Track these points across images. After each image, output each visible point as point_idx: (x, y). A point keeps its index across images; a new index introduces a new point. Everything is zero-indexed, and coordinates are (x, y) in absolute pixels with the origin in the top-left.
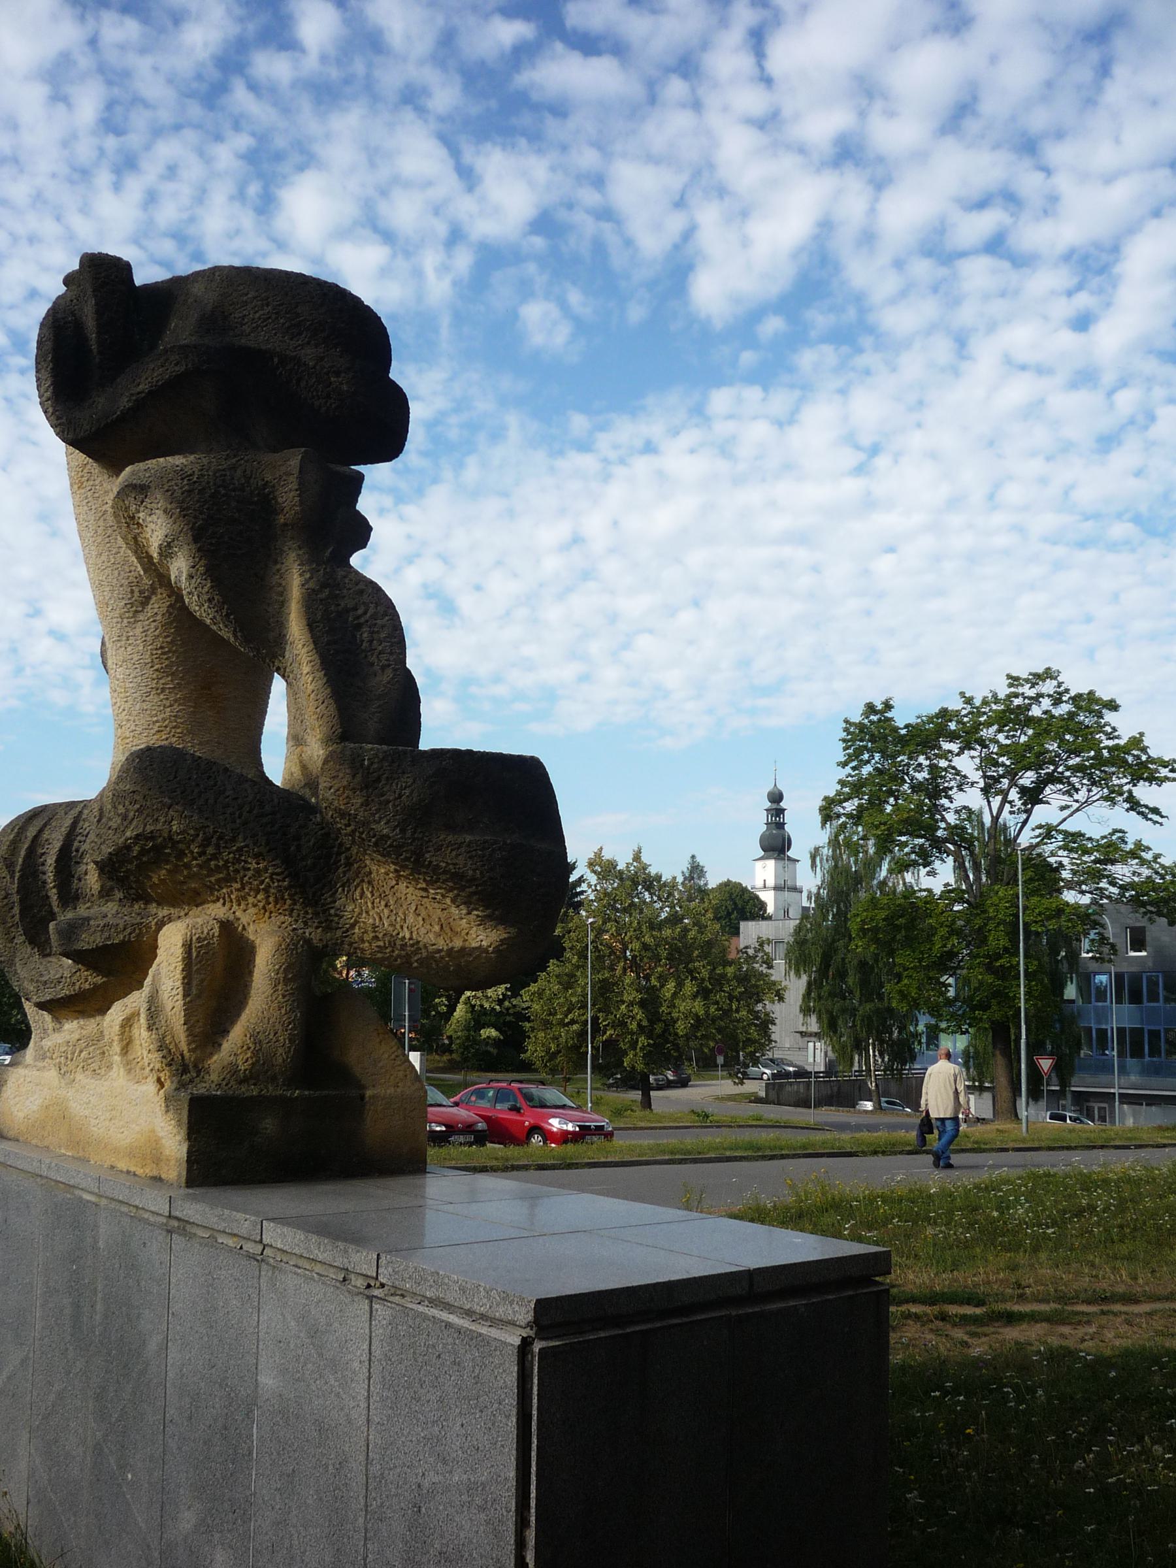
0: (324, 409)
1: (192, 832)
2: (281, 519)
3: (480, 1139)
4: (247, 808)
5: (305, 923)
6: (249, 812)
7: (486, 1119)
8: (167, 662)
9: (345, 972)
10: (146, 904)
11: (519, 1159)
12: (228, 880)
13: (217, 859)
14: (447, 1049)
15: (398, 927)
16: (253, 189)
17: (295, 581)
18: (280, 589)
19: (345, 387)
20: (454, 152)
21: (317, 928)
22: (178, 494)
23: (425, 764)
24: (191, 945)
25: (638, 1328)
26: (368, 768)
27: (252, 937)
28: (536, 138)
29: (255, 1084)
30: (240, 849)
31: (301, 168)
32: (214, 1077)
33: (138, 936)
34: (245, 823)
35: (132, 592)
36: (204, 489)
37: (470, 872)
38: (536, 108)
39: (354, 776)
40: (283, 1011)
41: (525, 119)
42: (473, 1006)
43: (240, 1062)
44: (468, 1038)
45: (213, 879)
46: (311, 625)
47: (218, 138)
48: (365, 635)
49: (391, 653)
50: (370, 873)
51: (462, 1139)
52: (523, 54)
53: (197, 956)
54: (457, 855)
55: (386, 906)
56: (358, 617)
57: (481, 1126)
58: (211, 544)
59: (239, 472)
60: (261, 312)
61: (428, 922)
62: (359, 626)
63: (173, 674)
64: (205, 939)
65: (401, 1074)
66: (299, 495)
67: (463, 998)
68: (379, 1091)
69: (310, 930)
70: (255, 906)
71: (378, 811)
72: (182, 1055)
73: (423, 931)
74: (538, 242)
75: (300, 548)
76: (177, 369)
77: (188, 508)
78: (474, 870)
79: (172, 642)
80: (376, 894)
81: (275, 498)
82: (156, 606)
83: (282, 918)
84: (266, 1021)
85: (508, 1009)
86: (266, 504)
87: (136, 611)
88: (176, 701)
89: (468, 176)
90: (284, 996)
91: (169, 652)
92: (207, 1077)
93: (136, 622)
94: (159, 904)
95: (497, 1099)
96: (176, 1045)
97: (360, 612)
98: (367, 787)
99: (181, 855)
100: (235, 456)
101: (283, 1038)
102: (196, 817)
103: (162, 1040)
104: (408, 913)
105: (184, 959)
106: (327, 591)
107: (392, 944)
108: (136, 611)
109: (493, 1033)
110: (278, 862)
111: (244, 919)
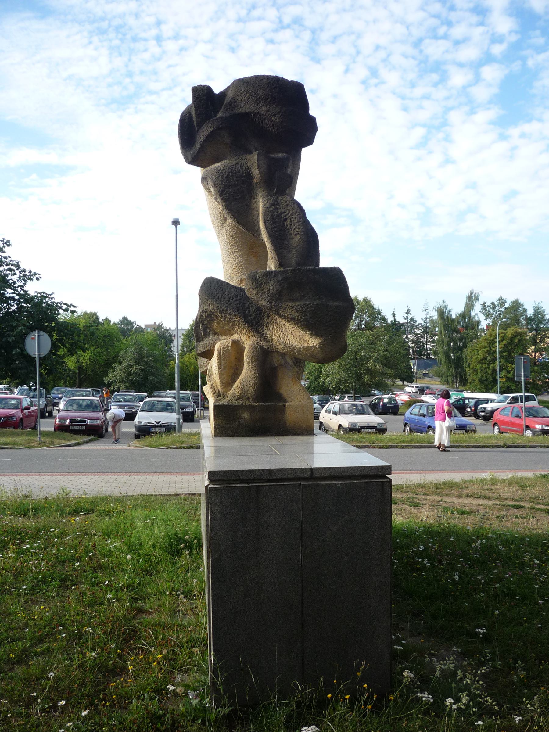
2: (255, 181)
9: (534, 354)
19: (278, 121)
25: (255, 485)
30: (230, 314)
34: (231, 304)
35: (221, 216)
46: (265, 223)
49: (299, 229)
54: (292, 311)
56: (286, 216)
62: (286, 220)
63: (237, 246)
65: (302, 397)
68: (293, 403)
71: (261, 296)
73: (294, 341)
78: (298, 316)
81: (252, 173)
86: (249, 176)
88: (239, 256)
97: (286, 213)
98: (257, 287)
99: (217, 317)
105: (218, 355)
106: (273, 207)
110: (242, 317)
111: (244, 339)
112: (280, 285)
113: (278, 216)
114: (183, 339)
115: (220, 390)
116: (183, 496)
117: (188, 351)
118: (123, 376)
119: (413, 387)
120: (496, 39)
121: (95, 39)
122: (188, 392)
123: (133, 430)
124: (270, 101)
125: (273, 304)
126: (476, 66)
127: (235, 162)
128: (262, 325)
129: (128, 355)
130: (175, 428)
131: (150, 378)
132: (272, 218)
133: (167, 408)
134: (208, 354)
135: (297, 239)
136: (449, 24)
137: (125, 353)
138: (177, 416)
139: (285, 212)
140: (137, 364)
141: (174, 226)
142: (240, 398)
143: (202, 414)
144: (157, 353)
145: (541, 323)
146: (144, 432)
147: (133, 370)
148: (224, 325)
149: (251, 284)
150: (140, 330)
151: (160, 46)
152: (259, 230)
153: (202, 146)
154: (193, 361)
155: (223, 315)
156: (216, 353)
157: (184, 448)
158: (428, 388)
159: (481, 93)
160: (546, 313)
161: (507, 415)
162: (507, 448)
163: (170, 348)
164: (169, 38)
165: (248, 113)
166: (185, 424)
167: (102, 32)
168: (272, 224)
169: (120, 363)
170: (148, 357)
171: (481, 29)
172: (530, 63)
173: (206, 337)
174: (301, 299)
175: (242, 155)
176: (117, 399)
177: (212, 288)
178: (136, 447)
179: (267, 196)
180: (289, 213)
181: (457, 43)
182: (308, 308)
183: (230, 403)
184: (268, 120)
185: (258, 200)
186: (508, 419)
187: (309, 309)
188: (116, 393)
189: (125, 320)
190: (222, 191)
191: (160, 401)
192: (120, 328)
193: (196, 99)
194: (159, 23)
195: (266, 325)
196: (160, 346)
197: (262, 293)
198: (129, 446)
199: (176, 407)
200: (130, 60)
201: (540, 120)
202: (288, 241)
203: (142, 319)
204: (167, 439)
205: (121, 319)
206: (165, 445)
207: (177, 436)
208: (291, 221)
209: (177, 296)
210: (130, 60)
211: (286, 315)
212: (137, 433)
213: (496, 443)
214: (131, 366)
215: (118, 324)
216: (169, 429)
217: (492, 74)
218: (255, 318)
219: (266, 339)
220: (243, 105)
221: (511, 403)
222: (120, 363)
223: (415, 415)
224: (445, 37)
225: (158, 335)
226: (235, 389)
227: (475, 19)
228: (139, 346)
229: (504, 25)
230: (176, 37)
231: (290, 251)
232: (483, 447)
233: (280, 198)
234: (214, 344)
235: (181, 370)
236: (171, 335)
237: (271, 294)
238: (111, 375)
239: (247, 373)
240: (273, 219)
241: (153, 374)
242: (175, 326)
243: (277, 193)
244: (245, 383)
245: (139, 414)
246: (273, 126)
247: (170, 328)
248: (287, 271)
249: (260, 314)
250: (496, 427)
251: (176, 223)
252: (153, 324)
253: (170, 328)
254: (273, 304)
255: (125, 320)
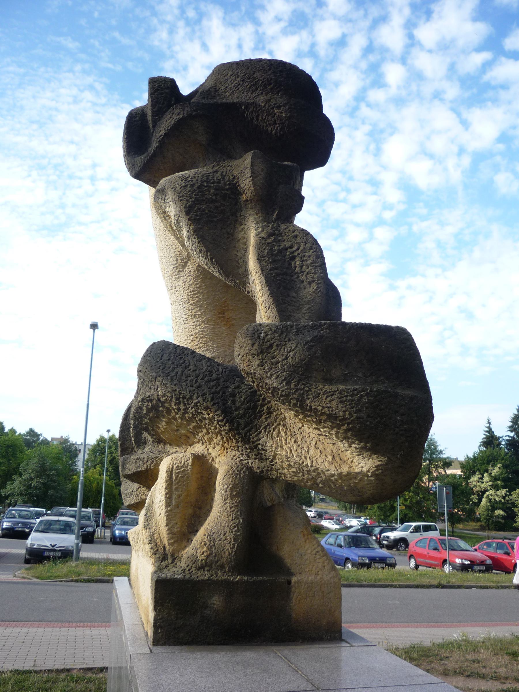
0: (273, 132)
1: (169, 395)
2: (244, 197)
3: (488, 569)
4: (201, 376)
5: (248, 456)
6: (202, 379)
7: (491, 558)
8: (197, 299)
9: (427, 483)
10: (164, 445)
11: (505, 582)
12: (199, 427)
13: (187, 413)
14: (478, 520)
15: (303, 457)
16: (372, 147)
17: (252, 232)
18: (245, 240)
19: (284, 115)
20: (459, 115)
21: (255, 459)
22: (178, 188)
23: (306, 333)
24: (172, 471)
26: (264, 339)
27: (217, 466)
28: (495, 101)
29: (208, 571)
30: (196, 405)
31: (392, 134)
32: (183, 564)
33: (155, 465)
34: (199, 387)
35: (177, 260)
36: (194, 184)
37: (341, 414)
38: (494, 88)
39: (253, 345)
40: (230, 518)
41: (491, 94)
42: (491, 499)
43: (199, 554)
44: (488, 515)
45: (191, 427)
46: (260, 259)
47: (356, 128)
48: (298, 263)
49: (315, 273)
50: (285, 418)
51: (478, 568)
52: (487, 66)
53: (176, 479)
54: (331, 401)
55: (295, 442)
56: (293, 252)
57: (489, 562)
58: (197, 215)
59: (219, 173)
60: (235, 83)
61: (324, 453)
62: (293, 258)
63: (200, 306)
64: (182, 467)
65: (320, 565)
66: (252, 180)
67: (485, 495)
68: (303, 577)
69: (252, 460)
70: (218, 444)
72: (164, 547)
73: (320, 460)
74: (501, 147)
75: (257, 214)
76: (178, 117)
77: (183, 196)
78: (344, 412)
79: (200, 287)
80: (289, 434)
81: (239, 185)
82: (190, 267)
83: (234, 453)
84: (219, 525)
85: (508, 501)
86: (234, 190)
87: (179, 271)
88: (202, 322)
89: (465, 124)
90: (231, 508)
91: (198, 293)
92: (178, 564)
93: (179, 277)
94: (170, 445)
95: (497, 548)
96: (161, 540)
97: (294, 249)
99: (169, 411)
100: (218, 165)
101: (230, 537)
102: (169, 384)
103: (152, 536)
104: (309, 446)
105: (167, 481)
106: (273, 238)
107: (301, 470)
108: (179, 271)
109: (501, 512)
110: (219, 412)
111: (214, 453)
112: (309, 349)
113: (280, 251)
114: (89, 454)
115: (167, 547)
116: (74, 673)
117: (92, 466)
118: (22, 489)
119: (312, 511)
120: (387, 207)
121: (34, 173)
122: (90, 510)
123: (24, 551)
124: (271, 89)
125: (293, 386)
126: (371, 227)
127: (211, 170)
128: (257, 428)
129: (30, 466)
130: (73, 553)
131: (51, 492)
132: (271, 252)
133: (66, 528)
134: (146, 478)
135: (311, 290)
136: (348, 191)
137: (27, 465)
138: (76, 541)
139: (291, 247)
140: (38, 476)
141: (92, 330)
142: (206, 566)
143: (103, 534)
144: (60, 467)
145: (434, 454)
146: (36, 556)
147: (34, 483)
148: (180, 426)
149: (249, 346)
150: (45, 442)
151: (93, 185)
152: (246, 274)
153: (162, 143)
154: (97, 476)
155: (182, 407)
156: (162, 476)
157: (81, 582)
158: (326, 513)
159: (374, 249)
160: (438, 444)
161: (424, 547)
162: (442, 588)
163: (75, 462)
164: (102, 179)
165: (237, 103)
166: (85, 545)
167: (42, 168)
168: (271, 263)
169: (21, 475)
170: (50, 470)
171: (375, 197)
172: (415, 228)
173: (138, 446)
174: (345, 380)
175: (224, 160)
176: (12, 514)
177: (165, 357)
178: (23, 578)
179: (263, 221)
180: (298, 249)
181: (354, 206)
182: (362, 396)
183: (188, 576)
184: (268, 115)
185: (246, 227)
186: (425, 552)
187: (365, 400)
188: (11, 508)
189: (31, 432)
190: (190, 206)
191: (58, 521)
192: (26, 439)
193: (155, 92)
194: (94, 166)
195: (265, 428)
196: (64, 460)
197: (272, 364)
198: (15, 576)
199: (76, 528)
200: (64, 194)
201: (424, 276)
202: (296, 292)
203: (49, 432)
204: (61, 568)
205: (28, 430)
206: (58, 576)
207: (74, 565)
208: (302, 261)
209: (88, 405)
210: (64, 194)
211: (320, 408)
212: (27, 557)
213: (429, 582)
214: (31, 479)
215: (24, 435)
216: (66, 555)
217: (383, 234)
218: (244, 414)
219: (260, 456)
220: (228, 94)
221: (413, 532)
222: (21, 475)
223: (331, 545)
224: (345, 201)
225: (63, 448)
226: (197, 546)
227: (369, 189)
228: (42, 459)
229: (394, 196)
230: (109, 178)
231: (299, 309)
232: (417, 587)
233: (283, 226)
234: (157, 461)
235: (85, 486)
236: (76, 450)
237: (289, 367)
238: (9, 487)
239: (220, 515)
240: (272, 255)
241: (54, 488)
242: (83, 441)
243: (278, 218)
244: (215, 536)
245: (33, 535)
246: (275, 123)
247: (76, 443)
248: (321, 325)
249: (255, 407)
250: (412, 560)
251: (94, 326)
252: (59, 437)
253: (76, 443)
254: (293, 386)
255: (31, 432)
